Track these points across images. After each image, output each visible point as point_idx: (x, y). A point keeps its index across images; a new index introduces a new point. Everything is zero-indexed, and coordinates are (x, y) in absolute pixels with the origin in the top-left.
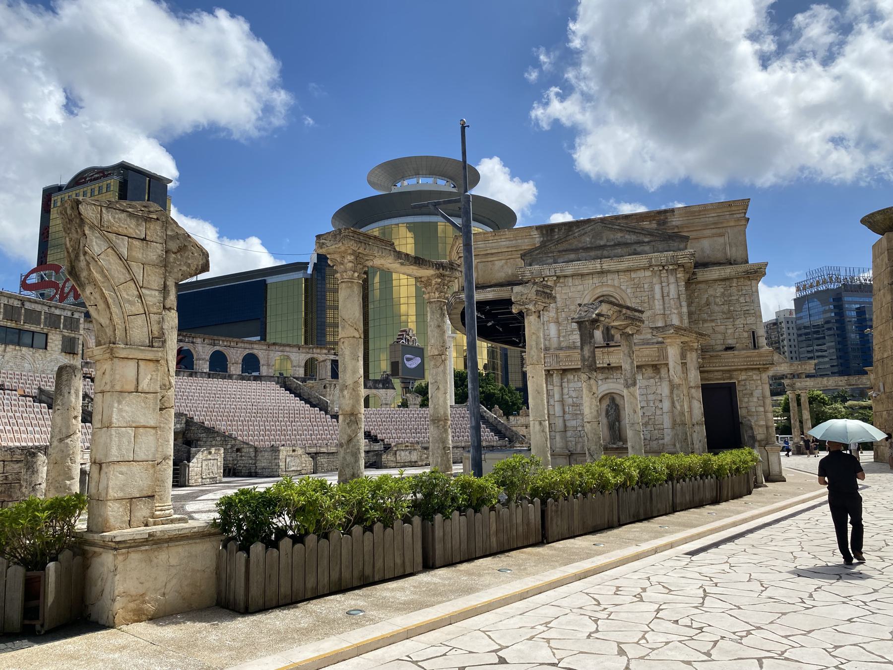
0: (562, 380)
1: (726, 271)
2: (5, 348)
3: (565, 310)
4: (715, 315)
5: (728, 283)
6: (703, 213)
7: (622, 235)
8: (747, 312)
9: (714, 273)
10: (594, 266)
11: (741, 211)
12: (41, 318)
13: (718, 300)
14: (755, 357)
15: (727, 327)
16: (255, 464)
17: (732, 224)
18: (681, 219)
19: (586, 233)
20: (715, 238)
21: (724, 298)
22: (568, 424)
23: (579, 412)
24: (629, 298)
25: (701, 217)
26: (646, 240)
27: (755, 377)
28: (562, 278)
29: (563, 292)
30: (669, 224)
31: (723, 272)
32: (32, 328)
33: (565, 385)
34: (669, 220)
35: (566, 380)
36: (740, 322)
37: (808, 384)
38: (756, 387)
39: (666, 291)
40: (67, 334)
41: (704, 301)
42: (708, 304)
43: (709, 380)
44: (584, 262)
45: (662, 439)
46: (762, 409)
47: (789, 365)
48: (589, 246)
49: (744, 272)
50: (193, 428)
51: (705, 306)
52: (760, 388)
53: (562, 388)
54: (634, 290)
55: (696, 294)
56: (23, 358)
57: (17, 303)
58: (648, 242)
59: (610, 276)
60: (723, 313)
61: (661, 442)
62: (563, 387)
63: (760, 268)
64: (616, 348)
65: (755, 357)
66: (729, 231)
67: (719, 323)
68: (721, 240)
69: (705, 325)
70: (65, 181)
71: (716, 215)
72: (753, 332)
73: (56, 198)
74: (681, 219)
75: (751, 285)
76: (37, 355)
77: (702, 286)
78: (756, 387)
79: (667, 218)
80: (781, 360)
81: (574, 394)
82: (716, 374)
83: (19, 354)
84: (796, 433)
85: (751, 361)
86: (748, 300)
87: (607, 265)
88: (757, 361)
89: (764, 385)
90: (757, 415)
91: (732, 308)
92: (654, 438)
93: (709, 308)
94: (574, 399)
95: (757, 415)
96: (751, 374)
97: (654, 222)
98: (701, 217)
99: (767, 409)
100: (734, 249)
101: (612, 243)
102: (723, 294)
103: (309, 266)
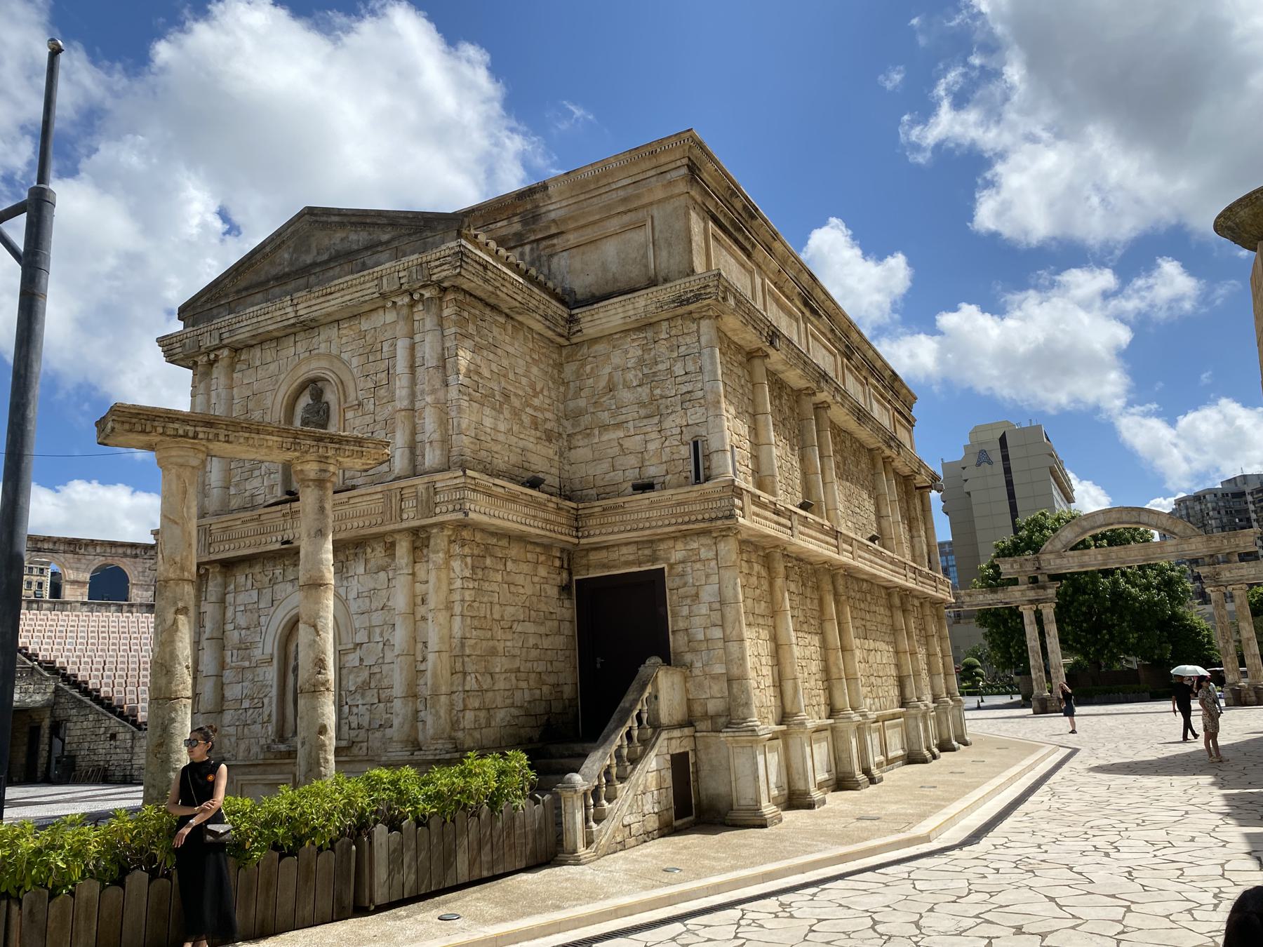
1: (637, 305)
4: (624, 410)
5: (650, 334)
6: (604, 181)
7: (344, 235)
8: (688, 397)
9: (613, 312)
10: (282, 312)
11: (679, 163)
13: (630, 376)
14: (694, 502)
15: (648, 437)
16: (130, 761)
17: (660, 194)
18: (564, 203)
19: (283, 242)
20: (629, 235)
21: (641, 370)
25: (603, 190)
26: (385, 237)
27: (704, 553)
28: (244, 351)
29: (245, 382)
30: (544, 219)
31: (631, 306)
33: (230, 598)
34: (544, 210)
35: (232, 586)
36: (673, 422)
37: (1244, 572)
38: (707, 576)
41: (602, 383)
42: (611, 388)
43: (609, 567)
44: (264, 305)
46: (717, 633)
47: (1205, 539)
48: (287, 270)
49: (674, 301)
50: (63, 700)
51: (605, 394)
52: (715, 579)
54: (363, 359)
55: (588, 368)
58: (388, 242)
59: (325, 333)
60: (642, 404)
63: (705, 287)
65: (694, 502)
66: (655, 214)
67: (632, 429)
68: (639, 237)
69: (605, 438)
71: (629, 181)
72: (696, 444)
74: (564, 203)
75: (698, 331)
77: (600, 348)
78: (707, 576)
79: (537, 207)
80: (1188, 532)
81: (242, 620)
82: (624, 550)
84: (1230, 666)
85: (685, 514)
86: (691, 368)
87: (308, 305)
88: (699, 512)
89: (727, 574)
90: (708, 649)
91: (658, 392)
93: (614, 397)
94: (243, 632)
95: (708, 649)
96: (695, 545)
97: (516, 219)
98: (603, 190)
99: (728, 632)
100: (664, 254)
101: (325, 257)
102: (641, 362)
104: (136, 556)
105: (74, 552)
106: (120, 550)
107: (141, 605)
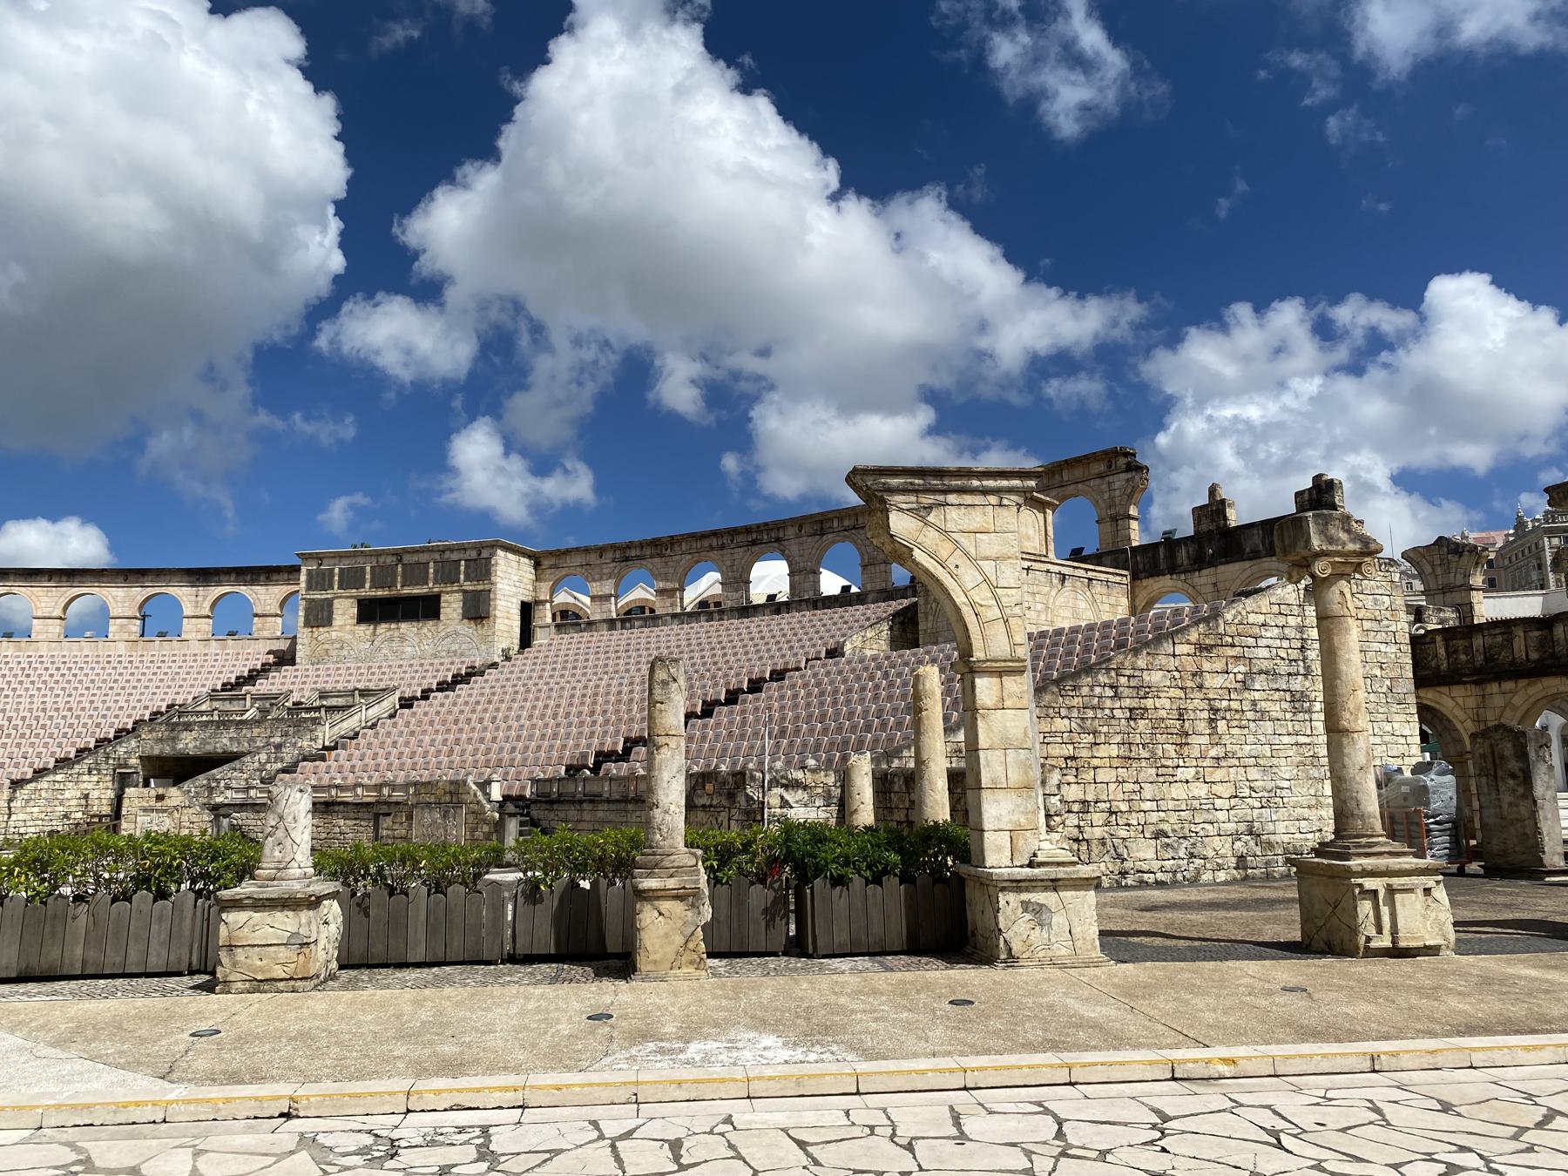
2: (375, 629)
12: (428, 573)
32: (415, 591)
40: (471, 588)
56: (403, 639)
83: (396, 634)
104: (722, 547)
105: (660, 555)
106: (706, 543)
107: (732, 609)
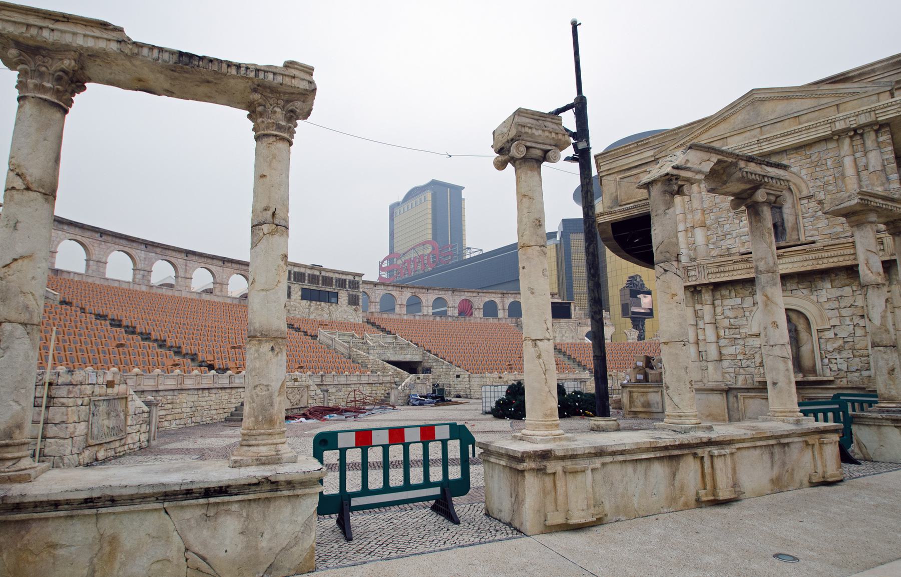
0: (713, 297)
3: (714, 210)
22: (724, 351)
23: (738, 336)
24: (805, 182)
39: (862, 162)
45: (867, 370)
53: (715, 307)
54: (810, 170)
57: (317, 273)
61: (866, 373)
62: (716, 305)
64: (787, 250)
70: (401, 199)
73: (397, 211)
76: (331, 308)
83: (320, 307)
92: (853, 368)
94: (732, 320)
103: (558, 234)
